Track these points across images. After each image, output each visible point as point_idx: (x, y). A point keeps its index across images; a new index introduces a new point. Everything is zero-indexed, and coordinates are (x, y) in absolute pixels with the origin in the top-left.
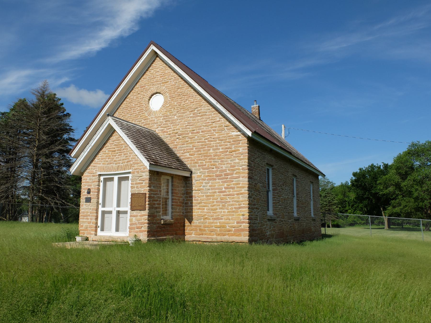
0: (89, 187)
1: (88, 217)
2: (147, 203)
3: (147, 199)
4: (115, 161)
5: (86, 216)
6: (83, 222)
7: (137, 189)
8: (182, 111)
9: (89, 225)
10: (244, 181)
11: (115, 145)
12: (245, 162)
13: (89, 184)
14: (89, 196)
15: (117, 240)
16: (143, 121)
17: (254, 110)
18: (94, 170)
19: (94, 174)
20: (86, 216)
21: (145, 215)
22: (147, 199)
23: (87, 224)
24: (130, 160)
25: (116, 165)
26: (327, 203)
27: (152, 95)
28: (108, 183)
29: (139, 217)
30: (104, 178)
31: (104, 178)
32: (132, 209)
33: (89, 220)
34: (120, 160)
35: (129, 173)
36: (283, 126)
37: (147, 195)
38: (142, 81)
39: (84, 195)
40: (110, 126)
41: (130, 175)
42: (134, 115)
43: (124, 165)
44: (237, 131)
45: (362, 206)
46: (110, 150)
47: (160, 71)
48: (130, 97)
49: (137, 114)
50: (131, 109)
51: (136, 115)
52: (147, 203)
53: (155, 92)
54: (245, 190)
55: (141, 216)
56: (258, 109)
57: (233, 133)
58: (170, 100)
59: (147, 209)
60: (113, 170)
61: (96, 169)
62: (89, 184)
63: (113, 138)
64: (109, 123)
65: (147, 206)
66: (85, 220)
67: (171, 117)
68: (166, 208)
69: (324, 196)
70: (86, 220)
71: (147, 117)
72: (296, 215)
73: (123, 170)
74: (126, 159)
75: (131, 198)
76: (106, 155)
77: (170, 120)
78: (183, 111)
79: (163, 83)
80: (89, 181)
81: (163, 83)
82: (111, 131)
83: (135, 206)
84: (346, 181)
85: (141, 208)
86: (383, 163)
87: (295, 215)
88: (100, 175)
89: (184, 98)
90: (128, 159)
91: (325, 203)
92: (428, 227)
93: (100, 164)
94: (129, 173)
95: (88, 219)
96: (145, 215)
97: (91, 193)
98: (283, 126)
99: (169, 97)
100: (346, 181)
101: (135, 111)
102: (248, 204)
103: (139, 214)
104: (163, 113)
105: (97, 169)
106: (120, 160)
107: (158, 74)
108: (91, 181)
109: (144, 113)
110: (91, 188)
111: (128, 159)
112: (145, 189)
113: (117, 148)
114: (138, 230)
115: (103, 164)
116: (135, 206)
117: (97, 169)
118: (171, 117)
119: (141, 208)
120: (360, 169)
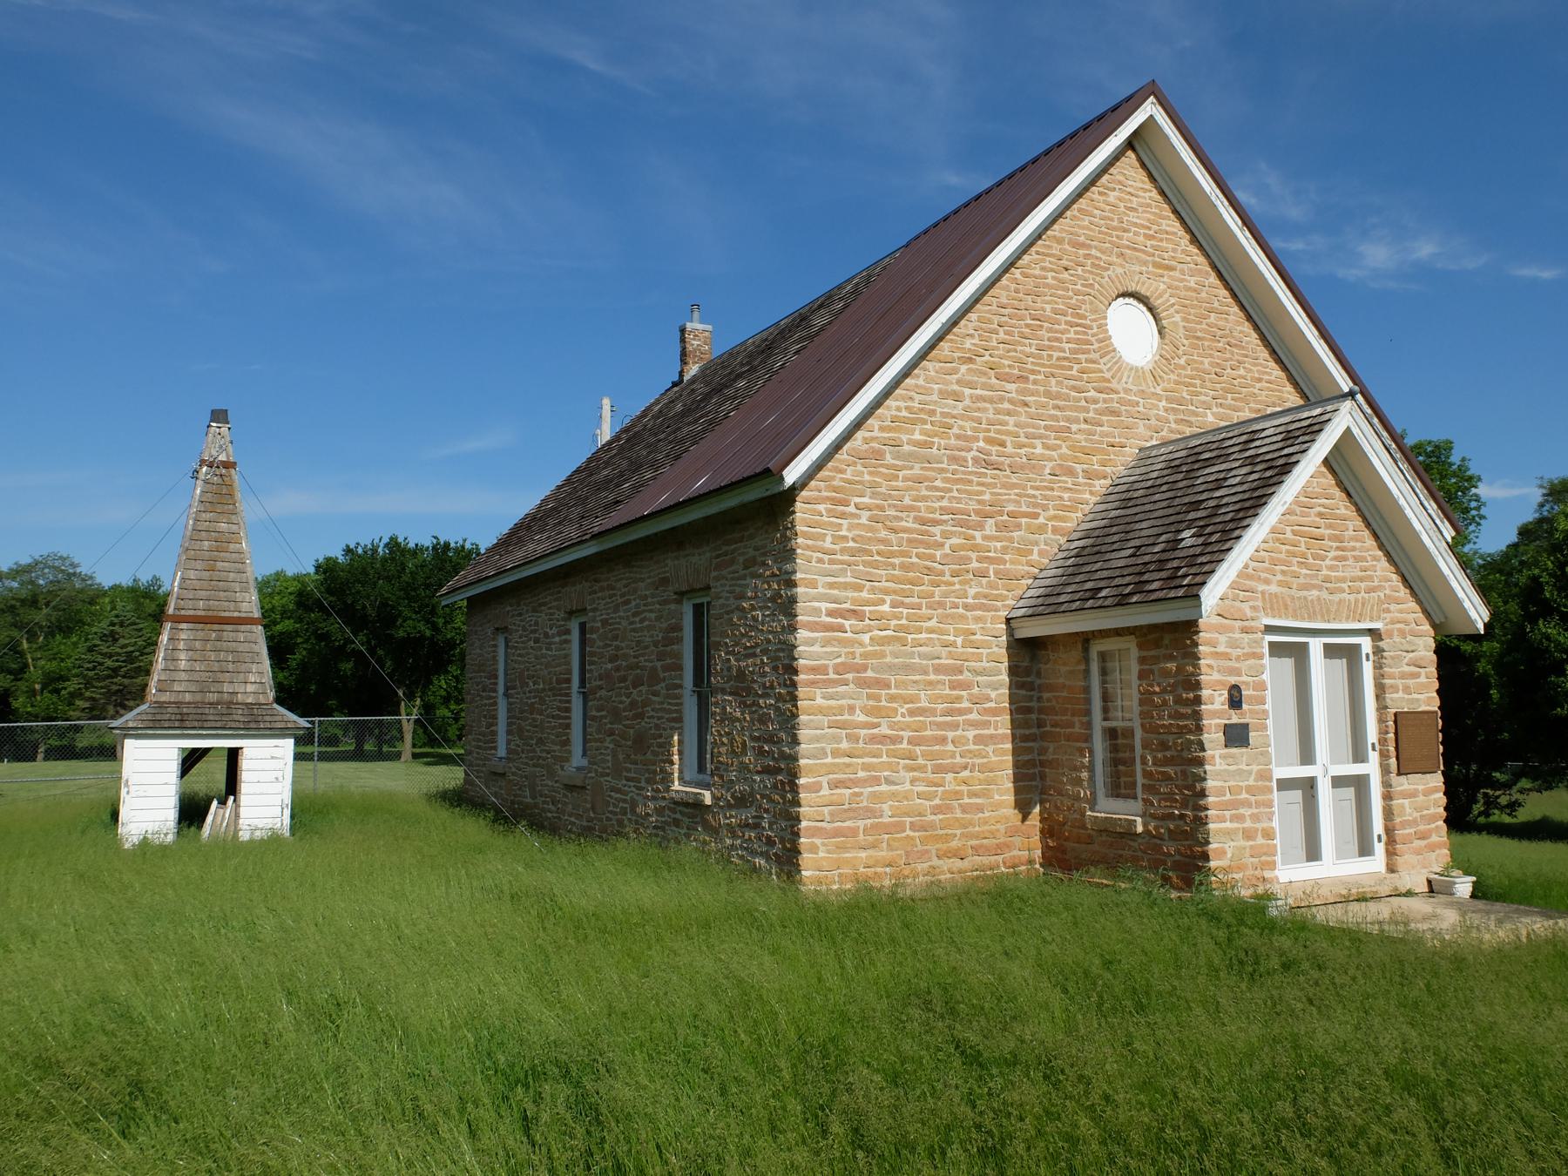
0: (1233, 680)
1: (1242, 811)
4: (1327, 580)
5: (1234, 805)
6: (1229, 833)
7: (1406, 696)
8: (1230, 401)
9: (1251, 847)
11: (1320, 515)
13: (1230, 663)
14: (1235, 720)
15: (1374, 889)
16: (1092, 393)
18: (1246, 607)
19: (1246, 623)
20: (1234, 805)
23: (1242, 843)
24: (1376, 584)
25: (1331, 597)
26: (117, 661)
29: (1421, 798)
33: (1248, 824)
34: (1343, 580)
36: (606, 403)
38: (1074, 218)
39: (1216, 714)
42: (1056, 354)
43: (1356, 601)
44: (1354, 509)
45: (286, 678)
46: (1305, 532)
47: (1140, 209)
48: (1028, 267)
49: (1067, 355)
50: (1041, 326)
51: (1065, 358)
55: (1427, 793)
58: (1185, 342)
60: (1323, 616)
61: (1251, 603)
62: (1230, 663)
66: (1228, 825)
67: (1194, 408)
68: (1114, 749)
69: (105, 635)
70: (1236, 825)
71: (1108, 381)
73: (1354, 620)
74: (1361, 580)
76: (1287, 547)
77: (1193, 419)
78: (1232, 402)
79: (1156, 265)
80: (1229, 650)
81: (1156, 265)
84: (154, 576)
86: (435, 537)
89: (1232, 353)
90: (1370, 578)
91: (109, 663)
92: (1547, 780)
93: (1267, 582)
95: (1240, 818)
97: (1244, 706)
98: (606, 403)
99: (1182, 331)
100: (154, 576)
101: (1058, 340)
103: (1421, 787)
104: (1165, 384)
105: (1259, 603)
106: (1343, 580)
107: (1135, 220)
108: (1239, 652)
109: (1094, 362)
110: (1243, 682)
111: (1370, 578)
113: (1330, 526)
114: (1423, 843)
115: (1280, 584)
117: (1259, 603)
118: (1194, 408)
120: (348, 551)
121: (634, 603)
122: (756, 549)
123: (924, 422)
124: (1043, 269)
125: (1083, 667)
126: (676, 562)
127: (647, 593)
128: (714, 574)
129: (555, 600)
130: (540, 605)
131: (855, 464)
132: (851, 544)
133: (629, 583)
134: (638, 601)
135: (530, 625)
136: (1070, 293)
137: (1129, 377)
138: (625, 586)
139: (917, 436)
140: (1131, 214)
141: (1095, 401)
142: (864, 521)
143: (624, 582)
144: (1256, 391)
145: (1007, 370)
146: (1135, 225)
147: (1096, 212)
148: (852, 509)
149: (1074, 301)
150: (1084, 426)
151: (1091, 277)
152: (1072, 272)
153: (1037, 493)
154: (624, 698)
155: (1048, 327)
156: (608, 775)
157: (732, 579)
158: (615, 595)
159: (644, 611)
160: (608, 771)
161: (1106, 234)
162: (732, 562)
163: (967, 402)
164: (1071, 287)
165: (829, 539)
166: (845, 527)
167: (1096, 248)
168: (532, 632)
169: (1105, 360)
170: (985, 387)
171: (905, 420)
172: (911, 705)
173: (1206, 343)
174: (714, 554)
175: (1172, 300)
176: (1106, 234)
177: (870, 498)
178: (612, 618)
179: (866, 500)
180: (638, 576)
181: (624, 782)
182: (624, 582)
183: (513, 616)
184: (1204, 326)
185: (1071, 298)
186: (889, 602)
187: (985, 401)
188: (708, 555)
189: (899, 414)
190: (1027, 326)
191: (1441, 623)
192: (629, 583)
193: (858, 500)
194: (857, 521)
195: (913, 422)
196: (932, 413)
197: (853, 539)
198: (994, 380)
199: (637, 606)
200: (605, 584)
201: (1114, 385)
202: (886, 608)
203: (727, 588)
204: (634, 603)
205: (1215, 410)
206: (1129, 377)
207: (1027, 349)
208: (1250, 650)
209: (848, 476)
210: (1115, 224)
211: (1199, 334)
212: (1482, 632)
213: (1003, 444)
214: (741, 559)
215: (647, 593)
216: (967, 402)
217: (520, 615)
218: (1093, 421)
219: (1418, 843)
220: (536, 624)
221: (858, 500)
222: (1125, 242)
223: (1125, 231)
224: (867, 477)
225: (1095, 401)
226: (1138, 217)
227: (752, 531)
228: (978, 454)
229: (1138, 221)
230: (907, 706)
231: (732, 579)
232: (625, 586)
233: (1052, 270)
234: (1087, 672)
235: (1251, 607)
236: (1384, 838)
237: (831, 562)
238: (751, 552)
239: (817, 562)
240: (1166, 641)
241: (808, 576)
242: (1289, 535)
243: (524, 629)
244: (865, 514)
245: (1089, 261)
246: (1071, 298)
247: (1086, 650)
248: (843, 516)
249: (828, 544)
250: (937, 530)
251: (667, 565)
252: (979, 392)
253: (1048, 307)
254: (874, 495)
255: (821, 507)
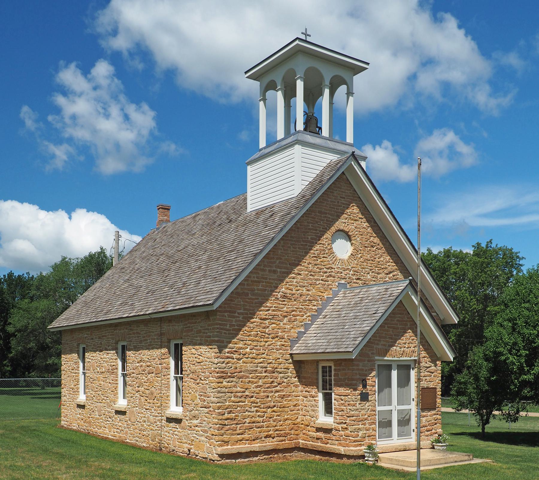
11: (398, 321)
16: (325, 270)
121: (149, 341)
122: (201, 327)
123: (263, 282)
124: (307, 222)
125: (316, 371)
126: (168, 328)
127: (155, 337)
128: (184, 334)
129: (111, 335)
130: (103, 336)
131: (238, 298)
132: (236, 327)
133: (147, 333)
134: (151, 340)
135: (98, 344)
136: (318, 232)
137: (339, 263)
138: (145, 334)
139: (260, 287)
140: (342, 199)
141: (326, 272)
142: (241, 319)
143: (145, 332)
144: (387, 266)
145: (293, 262)
146: (344, 204)
147: (329, 199)
148: (236, 314)
149: (319, 235)
150: (321, 282)
151: (326, 225)
152: (319, 223)
153: (303, 307)
154: (144, 378)
155: (309, 245)
156: (137, 407)
157: (192, 337)
158: (140, 337)
159: (153, 345)
160: (137, 405)
161: (332, 208)
162: (192, 330)
163: (279, 274)
164: (318, 229)
165: (228, 326)
166: (234, 321)
167: (328, 214)
168: (98, 347)
169: (330, 257)
170: (285, 268)
171: (256, 282)
172: (256, 384)
173: (369, 249)
174: (184, 327)
175: (357, 233)
176: (332, 208)
177: (243, 310)
178: (138, 345)
179: (242, 311)
180: (151, 330)
181: (144, 410)
182: (145, 332)
183: (89, 339)
184: (368, 242)
185: (318, 234)
186: (249, 348)
187: (285, 273)
188: (182, 327)
189: (254, 279)
190: (302, 245)
191: (440, 357)
192: (147, 333)
193: (239, 311)
194: (238, 319)
195: (259, 282)
196: (266, 279)
197: (237, 325)
198: (289, 266)
199: (150, 342)
200: (135, 331)
201: (333, 266)
202: (248, 350)
203: (190, 340)
204: (149, 341)
205: (371, 274)
206: (339, 263)
207: (301, 254)
208: (371, 368)
209: (235, 303)
210: (336, 203)
211: (366, 245)
212: (453, 361)
213: (291, 290)
214: (195, 330)
215: (155, 337)
216: (279, 274)
217: (92, 339)
218: (280, 429)
219: (427, 433)
220: (101, 344)
221: (239, 311)
222: (339, 211)
223: (340, 206)
224: (242, 303)
225: (326, 272)
226: (345, 201)
227: (200, 320)
228: (282, 293)
229: (345, 202)
230: (254, 385)
231: (192, 337)
232: (145, 334)
233: (312, 223)
234: (318, 373)
235: (371, 353)
236: (416, 430)
237: (229, 334)
238: (200, 328)
239: (224, 334)
240: (343, 364)
241: (221, 339)
242: (386, 328)
243: (94, 345)
244: (241, 316)
245: (326, 219)
246: (318, 234)
247: (318, 365)
248: (234, 317)
249: (228, 327)
250: (267, 322)
251: (164, 328)
252: (283, 270)
253: (309, 237)
254: (245, 309)
255: (226, 314)
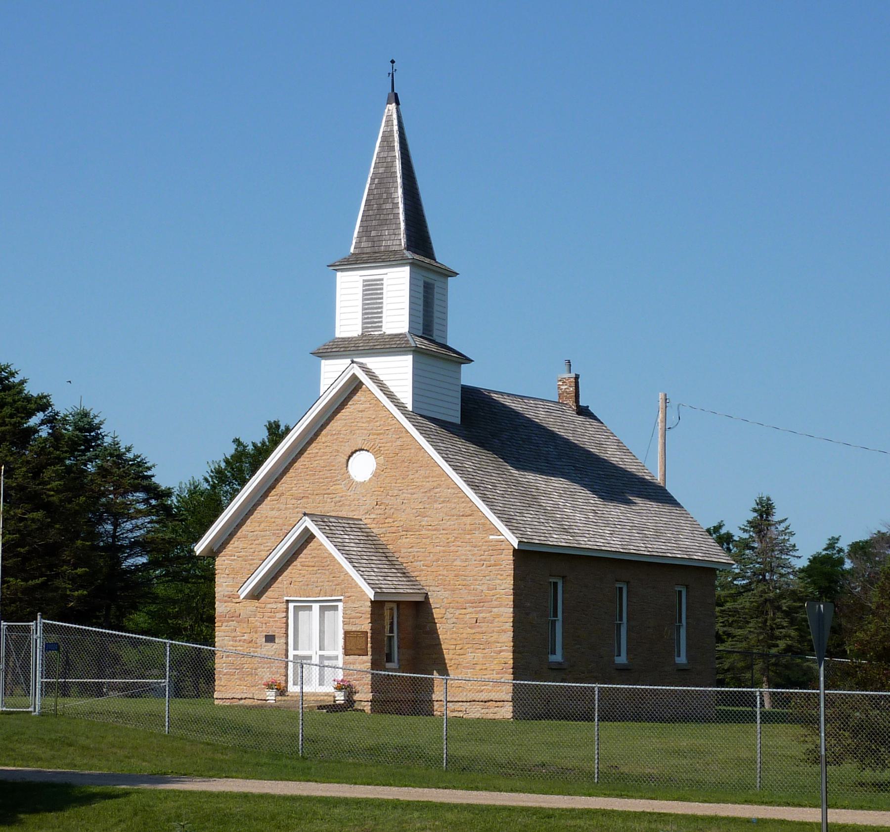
2: (369, 645)
3: (369, 639)
10: (506, 612)
12: (508, 583)
17: (564, 387)
21: (367, 662)
22: (369, 639)
27: (353, 453)
28: (302, 614)
30: (294, 606)
31: (294, 606)
32: (346, 653)
35: (340, 600)
37: (369, 635)
40: (306, 529)
41: (340, 605)
52: (369, 645)
53: (359, 446)
54: (509, 626)
56: (573, 384)
57: (491, 537)
59: (370, 653)
63: (312, 545)
64: (306, 527)
65: (369, 649)
72: (560, 659)
75: (345, 638)
82: (307, 538)
83: (351, 649)
85: (360, 652)
87: (682, 659)
88: (288, 601)
94: (340, 600)
96: (367, 662)
102: (513, 647)
112: (366, 625)
116: (351, 649)
119: (360, 652)
